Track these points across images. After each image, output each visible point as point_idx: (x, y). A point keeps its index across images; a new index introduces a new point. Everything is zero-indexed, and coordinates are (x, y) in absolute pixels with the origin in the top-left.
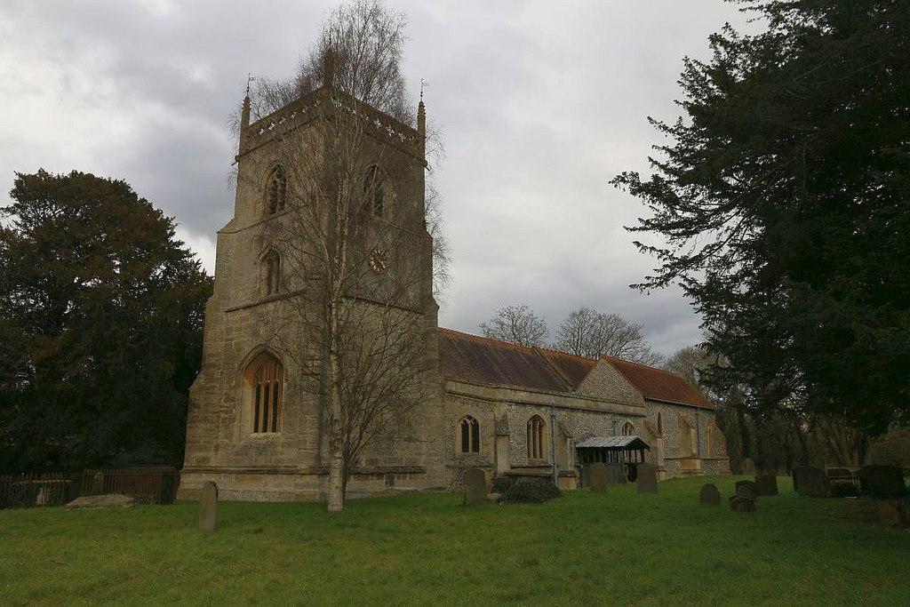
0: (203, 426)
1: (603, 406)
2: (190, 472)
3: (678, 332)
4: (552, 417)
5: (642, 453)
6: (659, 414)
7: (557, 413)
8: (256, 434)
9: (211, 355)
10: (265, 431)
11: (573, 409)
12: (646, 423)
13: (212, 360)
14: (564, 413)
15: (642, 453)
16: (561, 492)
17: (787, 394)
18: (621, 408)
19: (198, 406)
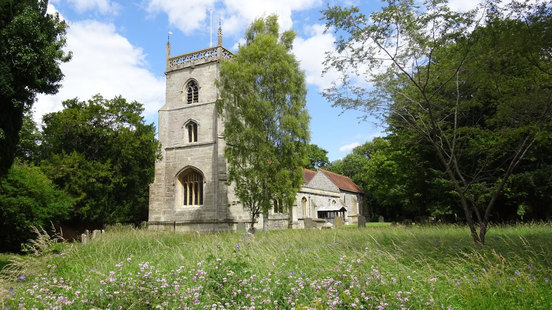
0: (157, 202)
1: (326, 193)
2: (152, 224)
3: (235, 49)
4: (309, 197)
5: (344, 213)
6: (339, 197)
7: (311, 196)
8: (185, 206)
9: (159, 169)
10: (191, 203)
11: (316, 194)
12: (340, 200)
13: (160, 172)
14: (313, 196)
15: (344, 213)
16: (360, 194)
17: (84, 206)
18: (332, 194)
19: (154, 193)
